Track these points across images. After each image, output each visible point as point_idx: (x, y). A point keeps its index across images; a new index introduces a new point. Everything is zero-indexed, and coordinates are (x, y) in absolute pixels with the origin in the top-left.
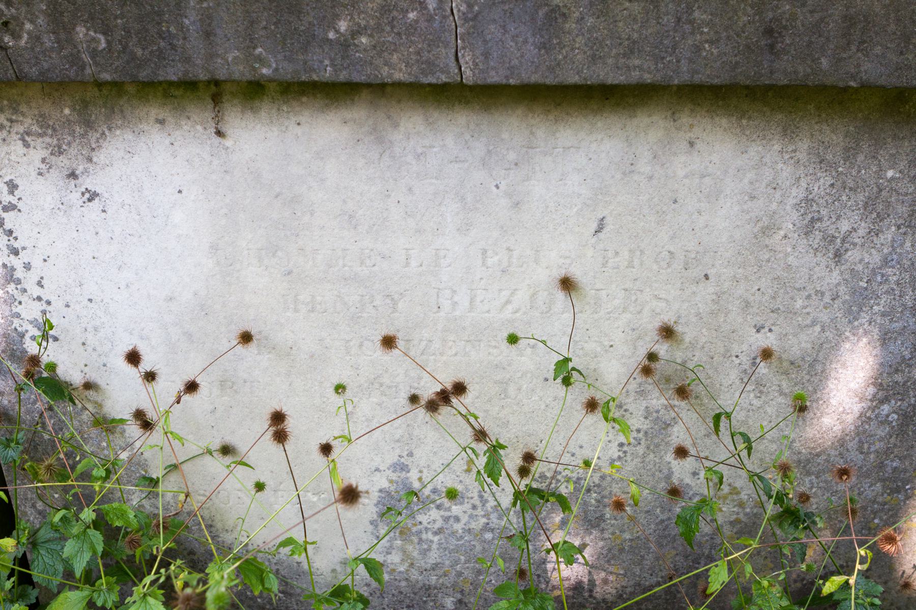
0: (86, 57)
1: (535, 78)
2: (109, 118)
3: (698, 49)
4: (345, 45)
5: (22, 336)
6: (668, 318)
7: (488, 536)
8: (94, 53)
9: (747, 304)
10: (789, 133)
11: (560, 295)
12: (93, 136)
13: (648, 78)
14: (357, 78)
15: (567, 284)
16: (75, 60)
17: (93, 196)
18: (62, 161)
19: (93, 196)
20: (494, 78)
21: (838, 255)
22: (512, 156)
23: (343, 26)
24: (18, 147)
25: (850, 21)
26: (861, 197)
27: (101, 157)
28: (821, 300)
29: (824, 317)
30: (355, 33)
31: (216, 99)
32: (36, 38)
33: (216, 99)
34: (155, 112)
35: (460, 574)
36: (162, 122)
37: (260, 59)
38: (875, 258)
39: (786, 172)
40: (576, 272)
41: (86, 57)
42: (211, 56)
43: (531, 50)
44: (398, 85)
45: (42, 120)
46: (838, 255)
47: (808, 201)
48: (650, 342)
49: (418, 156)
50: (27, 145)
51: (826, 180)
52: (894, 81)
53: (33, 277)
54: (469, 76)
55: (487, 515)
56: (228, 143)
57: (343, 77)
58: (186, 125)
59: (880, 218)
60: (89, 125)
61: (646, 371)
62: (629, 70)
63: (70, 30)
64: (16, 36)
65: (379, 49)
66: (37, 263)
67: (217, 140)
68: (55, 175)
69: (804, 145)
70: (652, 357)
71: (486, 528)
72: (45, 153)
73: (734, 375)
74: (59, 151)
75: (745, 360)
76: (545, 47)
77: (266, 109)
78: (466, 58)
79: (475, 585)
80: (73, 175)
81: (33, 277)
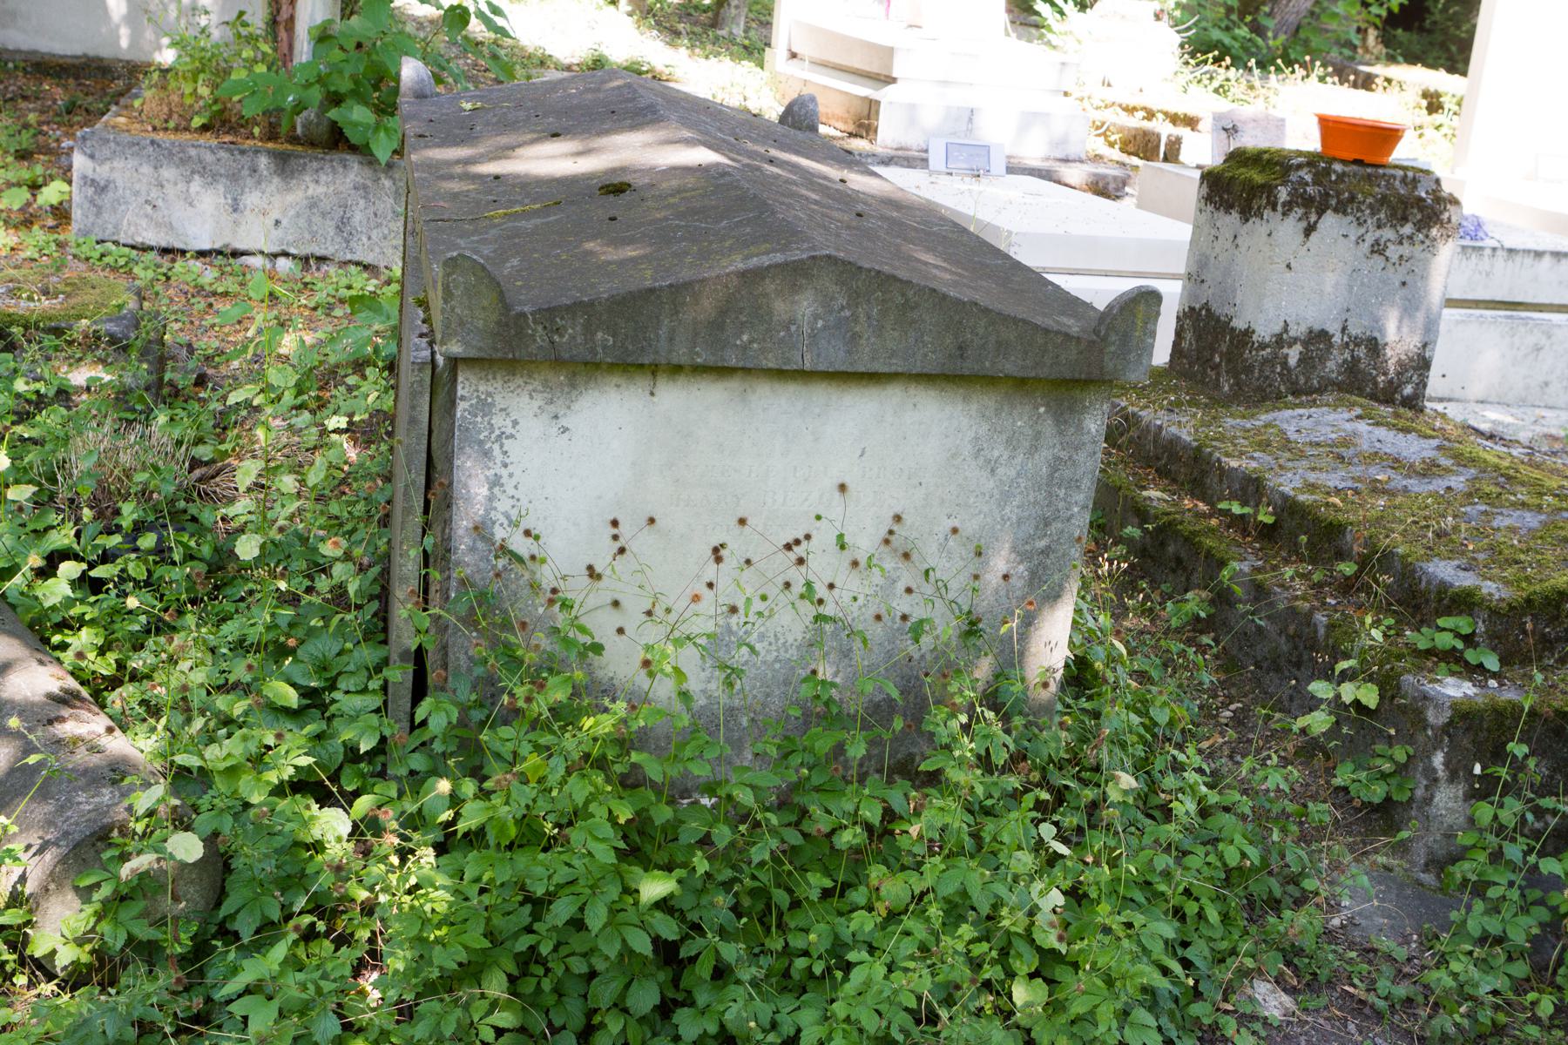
0: (600, 350)
1: (843, 368)
2: (587, 383)
3: (926, 355)
4: (745, 348)
5: (494, 523)
6: (898, 510)
7: (777, 666)
8: (605, 347)
9: (943, 501)
10: (966, 399)
11: (837, 494)
12: (575, 393)
13: (900, 370)
14: (749, 365)
15: (843, 488)
16: (593, 351)
17: (565, 430)
18: (552, 409)
19: (565, 430)
20: (822, 367)
21: (993, 471)
22: (817, 410)
23: (745, 338)
24: (526, 398)
25: (999, 343)
26: (1004, 437)
27: (575, 407)
28: (1215, 25)
29: (985, 509)
30: (751, 342)
31: (654, 374)
32: (573, 338)
33: (654, 374)
34: (615, 380)
35: (755, 697)
36: (618, 386)
37: (698, 354)
38: (1013, 473)
39: (965, 421)
40: (847, 481)
41: (600, 350)
42: (670, 351)
43: (842, 354)
44: (770, 370)
45: (545, 384)
46: (993, 471)
47: (977, 439)
48: (888, 523)
49: (764, 410)
50: (531, 397)
51: (985, 427)
52: (1021, 375)
53: (513, 482)
54: (808, 366)
55: (778, 650)
56: (655, 399)
57: (741, 364)
58: (632, 388)
59: (1015, 449)
60: (573, 386)
61: (887, 542)
62: (217, 74)
63: (593, 334)
64: (561, 336)
65: (763, 350)
66: (517, 473)
67: (649, 397)
68: (545, 417)
69: (974, 407)
70: (891, 532)
71: (777, 660)
72: (541, 403)
73: (934, 548)
74: (551, 402)
75: (941, 536)
76: (849, 352)
77: (682, 380)
78: (807, 357)
79: (764, 705)
80: (556, 417)
81: (513, 482)
